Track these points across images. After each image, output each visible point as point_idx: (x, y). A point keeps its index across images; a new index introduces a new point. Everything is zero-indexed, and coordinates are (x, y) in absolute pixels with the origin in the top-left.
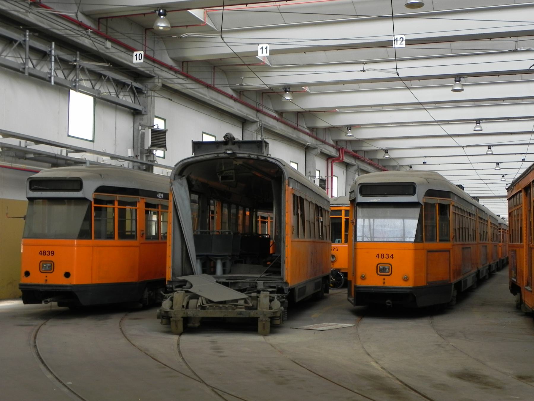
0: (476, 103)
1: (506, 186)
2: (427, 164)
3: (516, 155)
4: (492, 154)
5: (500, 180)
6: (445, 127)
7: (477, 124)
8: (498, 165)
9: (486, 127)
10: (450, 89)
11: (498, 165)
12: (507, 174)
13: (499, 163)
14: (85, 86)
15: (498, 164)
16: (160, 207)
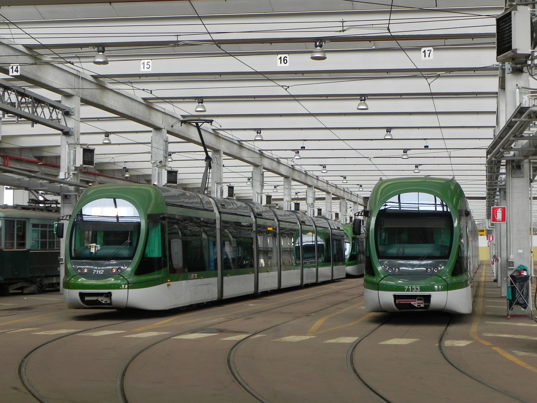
0: (331, 74)
1: (247, 181)
2: (429, 148)
3: (467, 140)
4: (262, 140)
5: (321, 171)
6: (304, 103)
7: (361, 101)
8: (298, 153)
9: (373, 105)
10: (309, 56)
12: (421, 165)
15: (170, 155)
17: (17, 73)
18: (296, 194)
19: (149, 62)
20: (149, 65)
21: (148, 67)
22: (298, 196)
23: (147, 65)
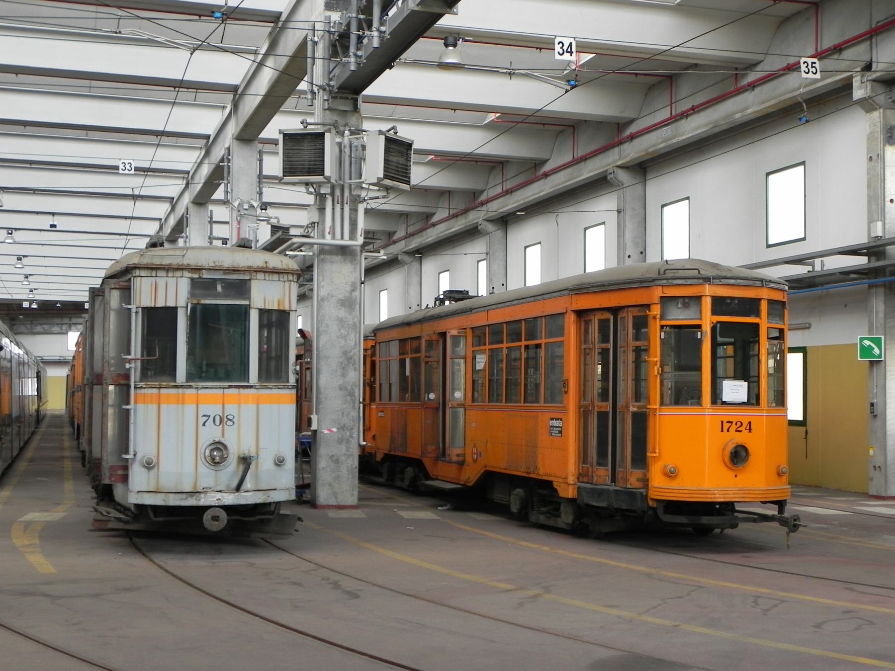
11: (21, 260)
13: (22, 257)
14: (435, 25)
16: (374, 359)
17: (571, 55)
18: (31, 291)
19: (815, 63)
20: (814, 67)
21: (814, 72)
22: (33, 294)
23: (812, 67)
